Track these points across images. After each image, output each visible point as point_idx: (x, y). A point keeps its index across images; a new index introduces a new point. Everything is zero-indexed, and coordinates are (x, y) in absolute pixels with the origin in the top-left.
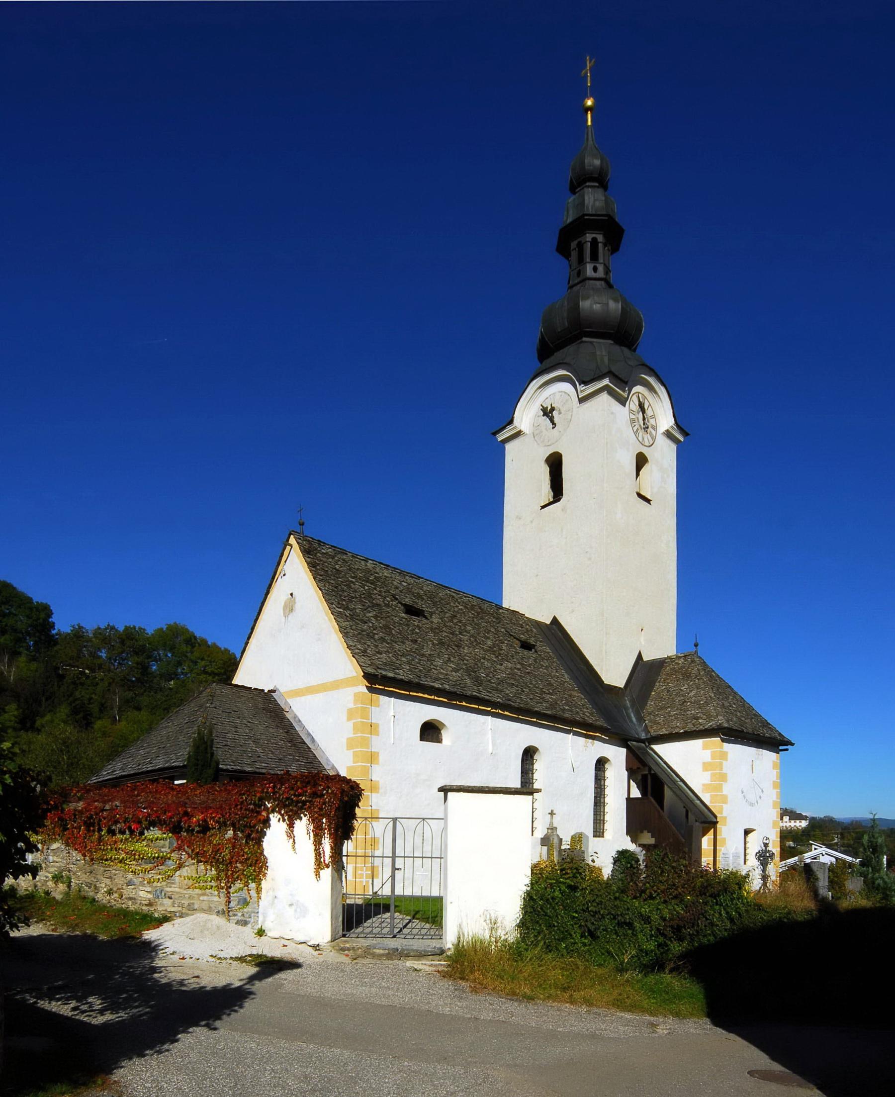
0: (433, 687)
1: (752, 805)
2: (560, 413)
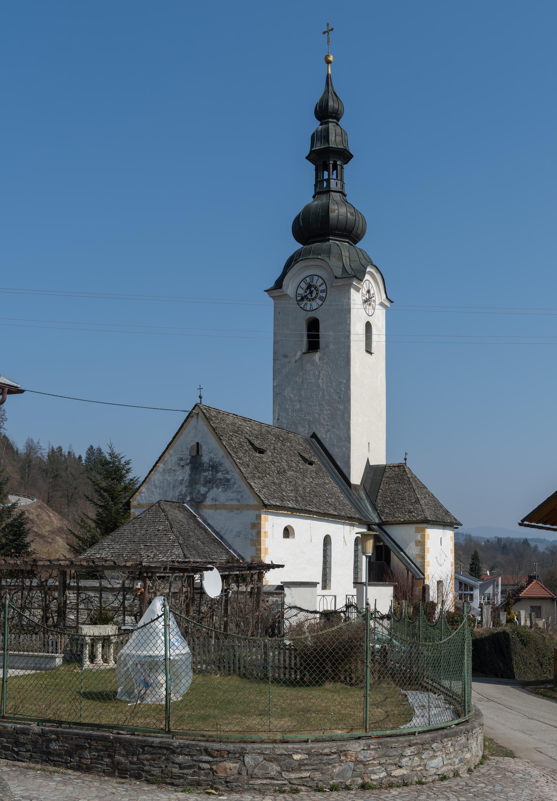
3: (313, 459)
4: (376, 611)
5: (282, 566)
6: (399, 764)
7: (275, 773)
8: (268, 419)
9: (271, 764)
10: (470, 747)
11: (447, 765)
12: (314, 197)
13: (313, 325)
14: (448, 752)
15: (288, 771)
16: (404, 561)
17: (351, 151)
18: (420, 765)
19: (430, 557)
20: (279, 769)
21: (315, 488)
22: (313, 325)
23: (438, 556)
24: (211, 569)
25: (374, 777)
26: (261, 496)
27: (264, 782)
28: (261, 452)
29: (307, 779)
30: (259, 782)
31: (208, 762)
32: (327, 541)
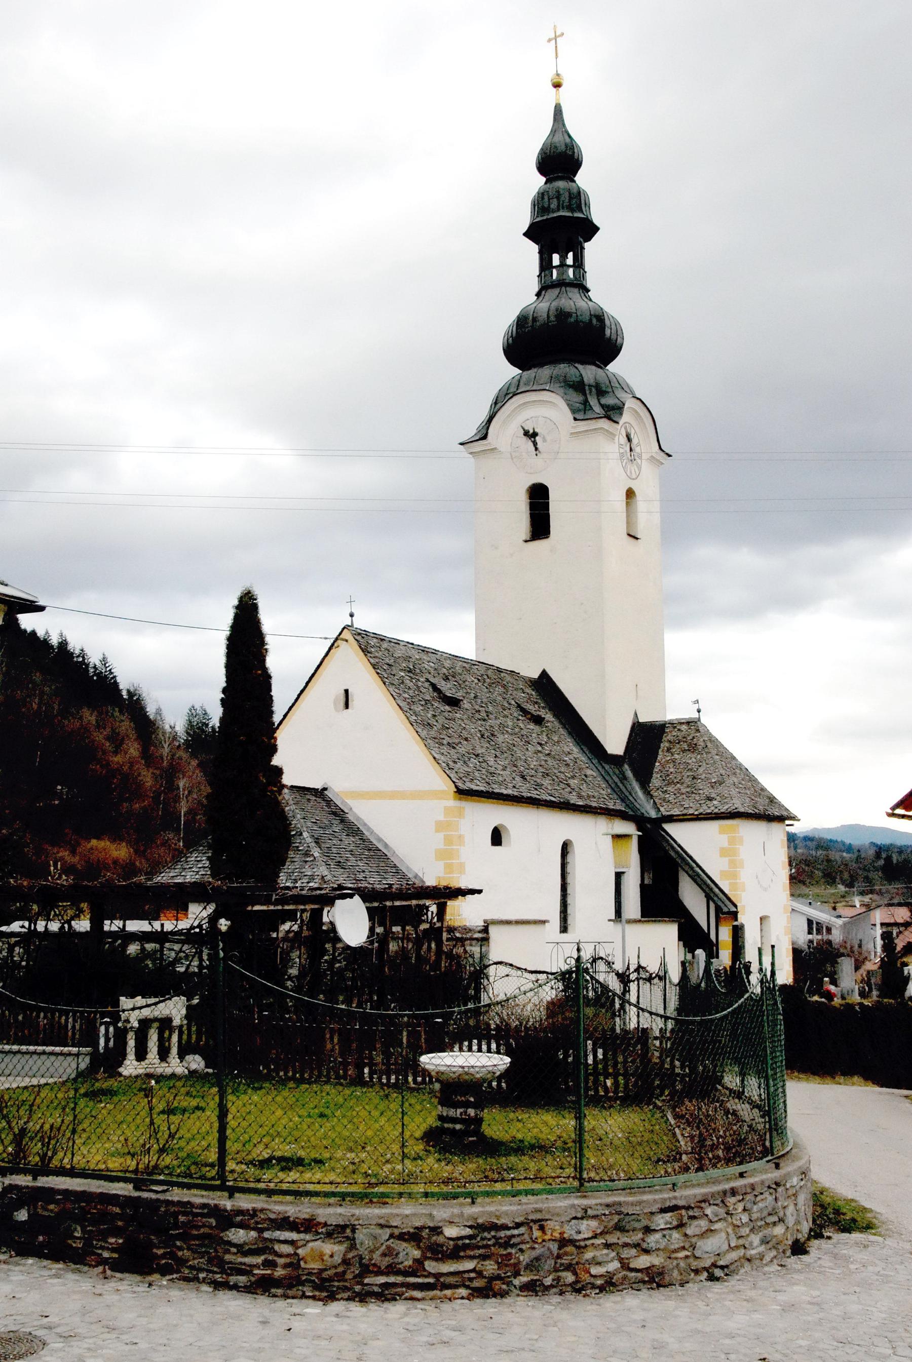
0: (502, 794)
1: (765, 890)
2: (544, 440)
3: (542, 713)
4: (639, 968)
5: (479, 892)
6: (644, 1246)
7: (411, 1263)
8: (20, 616)
9: (405, 1245)
10: (781, 1214)
11: (737, 1247)
12: (538, 295)
13: (539, 496)
14: (738, 1223)
15: (437, 1260)
16: (705, 883)
17: (596, 221)
18: (683, 1248)
19: (746, 876)
20: (417, 1254)
21: (546, 761)
22: (539, 496)
23: (750, 872)
24: (351, 896)
25: (594, 1270)
26: (452, 776)
27: (392, 1279)
28: (454, 702)
29: (473, 1275)
30: (382, 1280)
31: (292, 1243)
32: (566, 848)
